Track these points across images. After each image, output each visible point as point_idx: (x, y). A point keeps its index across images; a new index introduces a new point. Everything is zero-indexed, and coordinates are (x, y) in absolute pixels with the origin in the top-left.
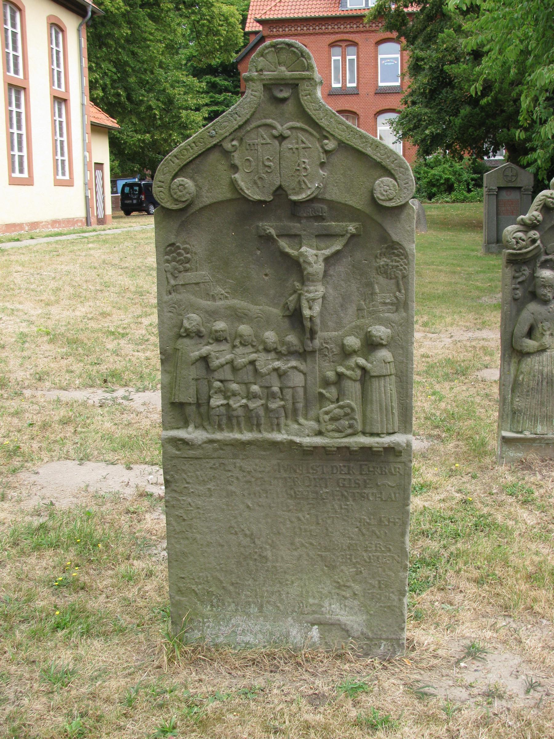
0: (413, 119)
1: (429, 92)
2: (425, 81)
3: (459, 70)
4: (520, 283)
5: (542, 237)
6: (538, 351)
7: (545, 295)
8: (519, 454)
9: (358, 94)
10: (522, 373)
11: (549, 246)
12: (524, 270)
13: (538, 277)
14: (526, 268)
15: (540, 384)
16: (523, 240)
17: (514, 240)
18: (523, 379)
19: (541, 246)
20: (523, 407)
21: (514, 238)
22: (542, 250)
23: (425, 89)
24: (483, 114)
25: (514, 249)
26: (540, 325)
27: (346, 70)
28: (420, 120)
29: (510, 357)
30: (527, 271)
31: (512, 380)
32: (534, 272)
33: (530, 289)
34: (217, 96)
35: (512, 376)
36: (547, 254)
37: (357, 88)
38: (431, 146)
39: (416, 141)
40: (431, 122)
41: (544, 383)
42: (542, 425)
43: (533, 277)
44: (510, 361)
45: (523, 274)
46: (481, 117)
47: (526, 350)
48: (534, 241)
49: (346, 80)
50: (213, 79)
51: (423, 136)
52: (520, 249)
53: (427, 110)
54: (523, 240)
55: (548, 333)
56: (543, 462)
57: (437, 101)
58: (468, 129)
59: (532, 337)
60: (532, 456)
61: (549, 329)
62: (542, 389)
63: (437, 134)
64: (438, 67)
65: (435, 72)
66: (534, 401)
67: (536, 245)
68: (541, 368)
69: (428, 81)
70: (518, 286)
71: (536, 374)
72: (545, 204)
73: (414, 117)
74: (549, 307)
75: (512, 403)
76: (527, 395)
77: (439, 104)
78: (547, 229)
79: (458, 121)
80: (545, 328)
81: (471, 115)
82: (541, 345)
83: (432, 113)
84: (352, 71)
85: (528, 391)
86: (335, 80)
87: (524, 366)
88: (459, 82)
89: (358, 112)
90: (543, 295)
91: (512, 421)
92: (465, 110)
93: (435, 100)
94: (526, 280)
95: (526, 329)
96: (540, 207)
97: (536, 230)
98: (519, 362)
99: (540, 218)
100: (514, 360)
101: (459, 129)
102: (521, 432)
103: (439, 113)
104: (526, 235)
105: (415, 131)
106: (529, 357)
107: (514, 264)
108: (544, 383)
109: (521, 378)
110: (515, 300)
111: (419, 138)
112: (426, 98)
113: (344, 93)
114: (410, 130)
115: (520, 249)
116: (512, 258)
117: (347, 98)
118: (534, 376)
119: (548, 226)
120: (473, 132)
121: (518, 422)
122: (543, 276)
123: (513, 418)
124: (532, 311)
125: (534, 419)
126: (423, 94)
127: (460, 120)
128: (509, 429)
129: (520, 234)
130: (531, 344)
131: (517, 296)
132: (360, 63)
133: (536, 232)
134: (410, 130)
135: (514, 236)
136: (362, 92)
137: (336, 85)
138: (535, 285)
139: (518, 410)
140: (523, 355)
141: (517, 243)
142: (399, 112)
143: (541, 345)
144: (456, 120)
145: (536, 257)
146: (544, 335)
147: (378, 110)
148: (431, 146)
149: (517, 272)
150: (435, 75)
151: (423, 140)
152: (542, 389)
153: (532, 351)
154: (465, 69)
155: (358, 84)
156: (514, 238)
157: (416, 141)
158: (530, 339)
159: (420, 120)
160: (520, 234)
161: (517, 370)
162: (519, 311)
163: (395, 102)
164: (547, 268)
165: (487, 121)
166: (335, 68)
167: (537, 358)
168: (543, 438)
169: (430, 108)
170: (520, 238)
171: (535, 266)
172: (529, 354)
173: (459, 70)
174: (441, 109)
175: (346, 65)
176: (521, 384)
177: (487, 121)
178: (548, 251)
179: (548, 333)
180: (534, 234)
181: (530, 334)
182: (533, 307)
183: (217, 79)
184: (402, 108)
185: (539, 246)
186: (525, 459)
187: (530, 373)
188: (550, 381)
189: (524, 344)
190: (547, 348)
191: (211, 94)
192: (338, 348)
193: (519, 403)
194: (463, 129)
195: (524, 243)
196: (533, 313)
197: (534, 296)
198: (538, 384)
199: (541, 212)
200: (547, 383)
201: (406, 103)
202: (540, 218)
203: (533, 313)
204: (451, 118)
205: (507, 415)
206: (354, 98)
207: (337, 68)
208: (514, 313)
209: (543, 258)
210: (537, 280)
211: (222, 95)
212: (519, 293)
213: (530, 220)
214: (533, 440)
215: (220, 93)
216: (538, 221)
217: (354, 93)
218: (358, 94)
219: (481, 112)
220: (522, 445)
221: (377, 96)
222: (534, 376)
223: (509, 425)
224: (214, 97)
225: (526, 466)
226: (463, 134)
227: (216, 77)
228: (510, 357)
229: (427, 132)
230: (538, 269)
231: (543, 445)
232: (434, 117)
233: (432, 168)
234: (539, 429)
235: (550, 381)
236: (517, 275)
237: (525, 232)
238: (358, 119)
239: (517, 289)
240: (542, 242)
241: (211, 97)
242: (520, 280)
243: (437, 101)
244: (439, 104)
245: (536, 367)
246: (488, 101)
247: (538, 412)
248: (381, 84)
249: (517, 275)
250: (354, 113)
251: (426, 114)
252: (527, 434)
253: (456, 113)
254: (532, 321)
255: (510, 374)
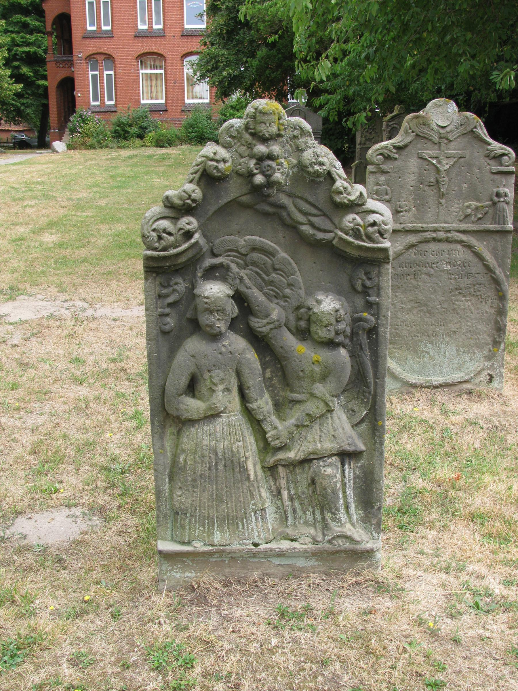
0: (211, 61)
1: (226, 33)
2: (222, 21)
3: (255, 10)
4: (170, 305)
5: (202, 227)
6: (206, 417)
7: (212, 326)
8: (188, 574)
9: (164, 36)
10: (183, 451)
11: (217, 242)
12: (176, 284)
13: (199, 296)
14: (181, 281)
15: (213, 468)
16: (170, 234)
17: (154, 234)
18: (185, 461)
19: (202, 242)
20: (188, 505)
21: (154, 230)
22: (205, 250)
23: (222, 30)
24: (280, 56)
25: (155, 249)
26: (206, 375)
27: (152, 12)
28: (218, 62)
29: (163, 427)
30: (181, 285)
31: (169, 461)
32: (193, 286)
33: (189, 315)
34: (28, 36)
35: (169, 454)
36: (215, 256)
37: (163, 29)
38: (229, 88)
39: (214, 83)
40: (228, 64)
41: (221, 467)
42: (221, 532)
43: (191, 295)
44: (163, 433)
45: (174, 290)
46: (279, 59)
47: (186, 415)
48: (188, 235)
49: (152, 22)
50: (24, 19)
51: (221, 78)
52: (165, 249)
53: (224, 51)
54: (170, 234)
55: (221, 387)
56: (225, 586)
57: (235, 42)
58: (265, 71)
59: (196, 393)
60: (207, 578)
61: (222, 381)
62: (217, 477)
63: (234, 76)
64: (235, 8)
65: (232, 13)
66: (206, 495)
67: (193, 241)
68: (213, 443)
69: (225, 22)
70: (167, 310)
71: (207, 453)
72: (205, 170)
73: (212, 58)
74: (220, 345)
75: (171, 498)
76: (193, 487)
77: (235, 46)
78: (211, 213)
79: (255, 63)
80: (215, 380)
81: (268, 57)
82: (210, 409)
83: (229, 54)
84: (158, 13)
85: (194, 480)
86: (141, 22)
87: (185, 439)
88: (256, 23)
89: (165, 55)
90: (208, 325)
91: (174, 526)
92: (262, 52)
93: (232, 41)
94: (181, 299)
95: (184, 381)
96: (197, 176)
97: (192, 215)
98: (179, 432)
99: (198, 194)
100: (170, 430)
101: (256, 71)
102: (189, 543)
103: (236, 54)
104: (175, 224)
105: (213, 73)
106: (193, 426)
107: (158, 274)
108: (221, 467)
109: (182, 460)
110: (164, 333)
111: (217, 79)
112: (223, 39)
113: (150, 35)
114: (208, 71)
115: (165, 249)
116: (152, 264)
117: (154, 40)
118: (203, 456)
119: (212, 208)
120: (270, 74)
121: (183, 527)
122: (207, 293)
123: (175, 520)
124: (193, 352)
125: (208, 522)
126: (220, 35)
127: (257, 62)
128: (169, 538)
129: (165, 224)
130: (193, 406)
131: (167, 328)
132: (166, 5)
133: (192, 219)
134: (208, 71)
135: (154, 226)
136: (168, 34)
137: (142, 27)
138: (196, 309)
139: (182, 510)
140: (184, 423)
141: (160, 238)
142: (197, 53)
143: (210, 409)
144: (253, 62)
145: (196, 260)
146: (214, 391)
147: (184, 53)
148: (229, 88)
149: (165, 287)
150: (231, 16)
151: (221, 82)
152: (217, 477)
153: (195, 417)
154: (260, 10)
155: (164, 26)
156: (154, 230)
157: (214, 83)
158: (194, 396)
159: (218, 62)
160: (165, 224)
161: (177, 446)
162: (173, 351)
163: (195, 45)
164: (215, 278)
165: (284, 63)
166: (141, 9)
167: (206, 428)
168: (224, 551)
169: (228, 49)
170: (164, 231)
171: (195, 276)
172: (192, 422)
173: (255, 10)
174: (239, 51)
175: (151, 7)
176: (183, 469)
177: (284, 63)
178: (215, 251)
179: (221, 387)
180: (189, 222)
181: (192, 387)
182: (194, 345)
183: (28, 19)
184: (201, 49)
185: (197, 243)
186: (198, 584)
187: (195, 453)
188: (229, 463)
189: (182, 407)
190: (222, 412)
191: (22, 34)
192: (174, 280)
193: (182, 498)
194: (261, 71)
195: (172, 238)
196: (193, 356)
197: (195, 326)
198: (210, 469)
199: (198, 184)
200: (225, 466)
201: (205, 44)
202: (198, 194)
203: (193, 356)
204: (249, 59)
205: (165, 516)
206: (160, 40)
207: (142, 9)
208: (164, 354)
209: (209, 262)
210: (198, 300)
211: (34, 36)
212: (171, 322)
213: (180, 198)
214: (210, 554)
215: (31, 33)
216: (194, 201)
217: (160, 35)
218: (164, 36)
219: (278, 54)
220: (192, 561)
221: (184, 39)
222: (203, 456)
223: (169, 532)
224: (25, 38)
225: (197, 596)
226: (260, 76)
227: (26, 16)
228: (163, 427)
229: (224, 73)
230: (200, 281)
231: (227, 559)
232: (232, 58)
233: (238, 110)
234: (217, 537)
235: (229, 463)
236: (165, 291)
237: (175, 219)
238: (165, 61)
239: (167, 315)
240: (204, 235)
241: (22, 38)
242: (170, 300)
243: (235, 42)
244: (235, 46)
245: (206, 442)
246: (275, 40)
247: (213, 512)
248: (187, 26)
249: (165, 291)
250: (161, 55)
251: (223, 55)
252: (199, 546)
253: (253, 55)
254: (192, 368)
255: (164, 454)
